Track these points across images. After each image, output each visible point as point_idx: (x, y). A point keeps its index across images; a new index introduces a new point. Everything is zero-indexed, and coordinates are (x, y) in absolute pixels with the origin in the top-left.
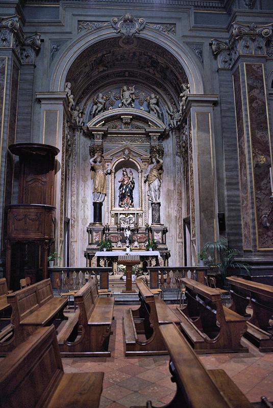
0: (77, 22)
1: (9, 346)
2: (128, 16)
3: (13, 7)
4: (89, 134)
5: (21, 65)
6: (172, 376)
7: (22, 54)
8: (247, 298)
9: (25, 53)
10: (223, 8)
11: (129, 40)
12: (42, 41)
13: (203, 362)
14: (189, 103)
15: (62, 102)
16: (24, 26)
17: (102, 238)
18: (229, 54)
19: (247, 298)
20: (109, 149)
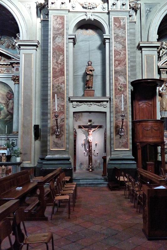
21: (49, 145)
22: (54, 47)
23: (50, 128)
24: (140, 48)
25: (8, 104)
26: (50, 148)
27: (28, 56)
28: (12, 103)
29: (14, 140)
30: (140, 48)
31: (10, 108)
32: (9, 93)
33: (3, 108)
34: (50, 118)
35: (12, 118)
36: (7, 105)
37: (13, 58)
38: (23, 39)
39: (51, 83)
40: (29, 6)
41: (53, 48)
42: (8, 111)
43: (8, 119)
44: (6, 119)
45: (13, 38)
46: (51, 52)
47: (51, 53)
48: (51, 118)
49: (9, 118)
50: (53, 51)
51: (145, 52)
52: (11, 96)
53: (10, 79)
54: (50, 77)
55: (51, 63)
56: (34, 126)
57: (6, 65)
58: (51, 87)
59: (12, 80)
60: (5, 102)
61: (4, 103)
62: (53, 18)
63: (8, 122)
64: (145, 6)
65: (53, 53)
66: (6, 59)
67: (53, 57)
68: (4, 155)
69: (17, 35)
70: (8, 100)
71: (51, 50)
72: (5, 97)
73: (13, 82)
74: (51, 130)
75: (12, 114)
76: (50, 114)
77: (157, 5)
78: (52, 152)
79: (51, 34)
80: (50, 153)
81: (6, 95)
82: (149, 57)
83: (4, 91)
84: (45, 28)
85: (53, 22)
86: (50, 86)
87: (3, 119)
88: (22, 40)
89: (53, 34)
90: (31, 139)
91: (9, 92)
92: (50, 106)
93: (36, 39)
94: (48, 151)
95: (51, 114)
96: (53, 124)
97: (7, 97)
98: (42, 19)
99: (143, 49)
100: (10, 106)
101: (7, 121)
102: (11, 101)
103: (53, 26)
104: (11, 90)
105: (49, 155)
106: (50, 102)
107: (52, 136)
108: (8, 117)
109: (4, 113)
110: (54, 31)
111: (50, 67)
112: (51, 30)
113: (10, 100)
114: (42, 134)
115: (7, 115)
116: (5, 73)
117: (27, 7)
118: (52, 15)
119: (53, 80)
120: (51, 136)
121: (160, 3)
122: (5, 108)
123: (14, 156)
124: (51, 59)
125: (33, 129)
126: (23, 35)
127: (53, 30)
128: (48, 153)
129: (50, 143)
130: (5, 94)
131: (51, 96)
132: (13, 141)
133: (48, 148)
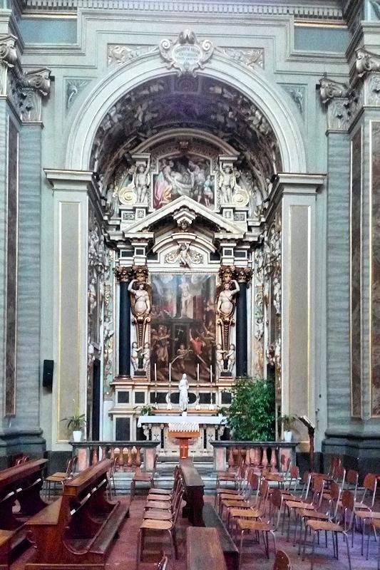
2: (187, 33)
11: (187, 80)
99: (56, 186)
121: (278, 83)
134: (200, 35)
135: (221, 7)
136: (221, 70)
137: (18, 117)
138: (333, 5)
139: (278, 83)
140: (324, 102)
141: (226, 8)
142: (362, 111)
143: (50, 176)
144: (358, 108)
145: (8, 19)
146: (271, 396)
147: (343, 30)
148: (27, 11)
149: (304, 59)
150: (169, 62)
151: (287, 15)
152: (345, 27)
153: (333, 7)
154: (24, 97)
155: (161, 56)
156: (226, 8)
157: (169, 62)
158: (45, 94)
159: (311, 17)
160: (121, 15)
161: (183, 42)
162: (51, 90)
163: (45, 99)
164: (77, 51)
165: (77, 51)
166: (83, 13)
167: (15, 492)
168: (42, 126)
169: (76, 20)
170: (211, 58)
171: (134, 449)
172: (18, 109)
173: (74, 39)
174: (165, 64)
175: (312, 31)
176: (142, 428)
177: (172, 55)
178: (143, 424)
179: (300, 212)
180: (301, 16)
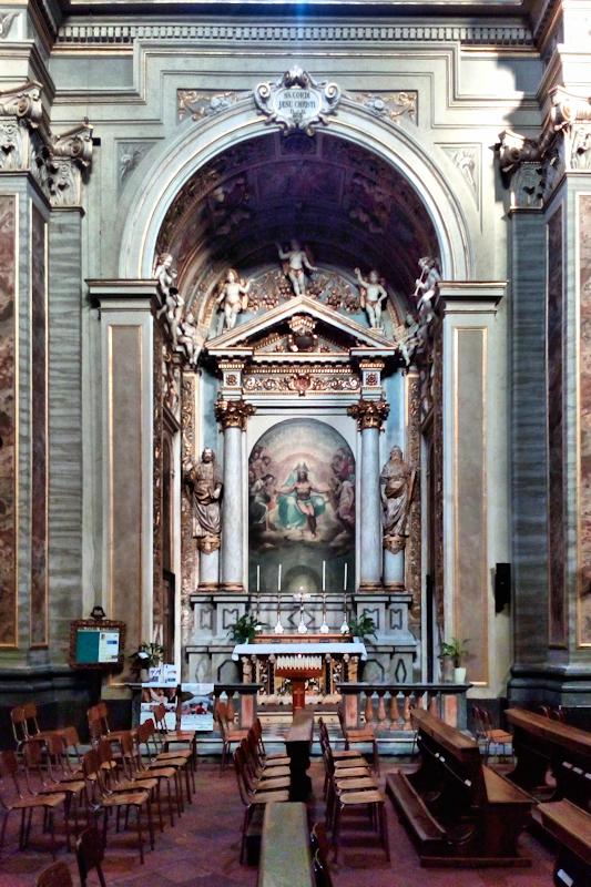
0: (175, 92)
1: (101, 836)
2: (296, 73)
3: (22, 57)
4: (210, 365)
5: (49, 207)
6: (308, 773)
7: (51, 182)
8: (565, 764)
9: (58, 180)
10: (528, 43)
11: (297, 139)
12: (97, 142)
13: (303, 830)
14: (438, 305)
15: (344, 798)
16: (51, 104)
17: (234, 585)
18: (539, 172)
19: (565, 764)
20: (240, 347)
21: (575, 632)
22: (585, 305)
23: (575, 575)
24: (95, 301)
25: (336, 493)
26: (577, 640)
27: (471, 337)
28: (351, 491)
29: (371, 609)
30: (95, 301)
31: (346, 509)
32: (341, 459)
33: (323, 508)
34: (575, 543)
35: (351, 540)
36: (336, 498)
37: (364, 343)
38: (453, 277)
39: (575, 423)
40: (467, 161)
41: (581, 306)
42: (338, 516)
43: (340, 544)
44: (332, 544)
45: (357, 271)
46: (574, 320)
47: (574, 324)
48: (579, 542)
49: (342, 540)
50: (581, 317)
51: (114, 315)
52: (346, 467)
53: (344, 411)
54: (574, 407)
55: (574, 357)
56: (494, 566)
57: (333, 365)
58: (575, 441)
59: (348, 415)
60: (327, 488)
61: (327, 492)
62: (581, 204)
63: (340, 552)
64: (119, 150)
65: (582, 324)
66: (331, 345)
67: (581, 337)
68: (356, 658)
69: (422, 263)
70: (337, 480)
71: (574, 314)
72: (329, 470)
73: (353, 423)
74: (579, 582)
75: (351, 528)
76: (575, 527)
77: (154, 143)
78: (580, 654)
79: (574, 260)
80: (577, 657)
81: (332, 466)
82: (126, 333)
83: (324, 450)
84: (522, 237)
85: (581, 218)
86: (575, 437)
87: (323, 541)
88: (464, 279)
89: (581, 259)
90: (486, 609)
91: (340, 453)
92: (575, 501)
93: (453, 277)
94: (572, 649)
95: (579, 528)
96: (585, 562)
97: (336, 472)
98: (513, 207)
99: (104, 304)
100: (346, 500)
101: (336, 549)
102: (346, 484)
103: (582, 233)
104: (347, 449)
105: (576, 661)
106: (575, 489)
107: (582, 600)
108: (340, 536)
109: (328, 523)
110: (584, 251)
111: (575, 373)
112: (574, 247)
113: (342, 480)
114: (517, 592)
115: (337, 531)
116: (327, 391)
117: (462, 163)
118: (578, 194)
119: (582, 417)
120: (579, 601)
121: (163, 138)
122: (329, 507)
123: (375, 664)
124: (575, 345)
125: (490, 579)
126: (454, 265)
127: (581, 246)
128: (571, 657)
129: (576, 624)
130: (329, 460)
131: (575, 469)
132: (369, 616)
133: (572, 640)
134: (316, 74)
135: (170, 29)
136: (351, 126)
137: (46, 201)
138: (518, 23)
139: (163, 138)
140: (506, 170)
141: (338, 32)
142: (564, 179)
143: (94, 290)
144: (558, 176)
145: (28, 53)
146: (279, 610)
147: (534, 59)
148: (58, 44)
149: (113, 99)
150: (268, 115)
151: (234, 40)
152: (536, 55)
153: (466, 26)
154: (53, 171)
155: (259, 106)
156: (262, 31)
157: (268, 115)
158: (85, 164)
159: (104, 39)
160: (261, 48)
161: (289, 83)
162: (95, 158)
163: (86, 174)
164: (132, 98)
165: (132, 98)
166: (143, 46)
167: (584, 773)
168: (81, 212)
169: (131, 57)
170: (337, 108)
171: (387, 696)
172: (45, 190)
173: (130, 81)
174: (264, 118)
175: (106, 62)
176: (240, 660)
177: (273, 107)
178: (240, 656)
179: (471, 337)
180: (507, 43)
